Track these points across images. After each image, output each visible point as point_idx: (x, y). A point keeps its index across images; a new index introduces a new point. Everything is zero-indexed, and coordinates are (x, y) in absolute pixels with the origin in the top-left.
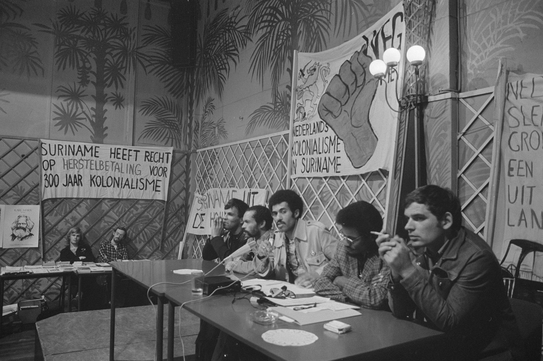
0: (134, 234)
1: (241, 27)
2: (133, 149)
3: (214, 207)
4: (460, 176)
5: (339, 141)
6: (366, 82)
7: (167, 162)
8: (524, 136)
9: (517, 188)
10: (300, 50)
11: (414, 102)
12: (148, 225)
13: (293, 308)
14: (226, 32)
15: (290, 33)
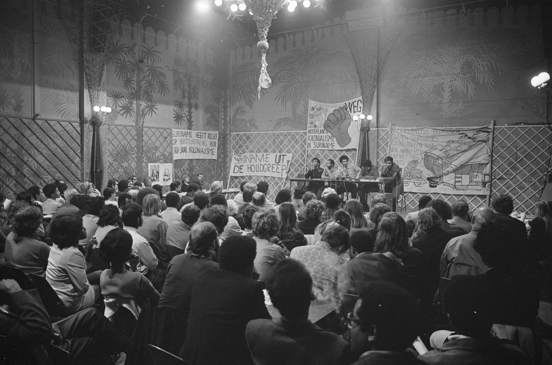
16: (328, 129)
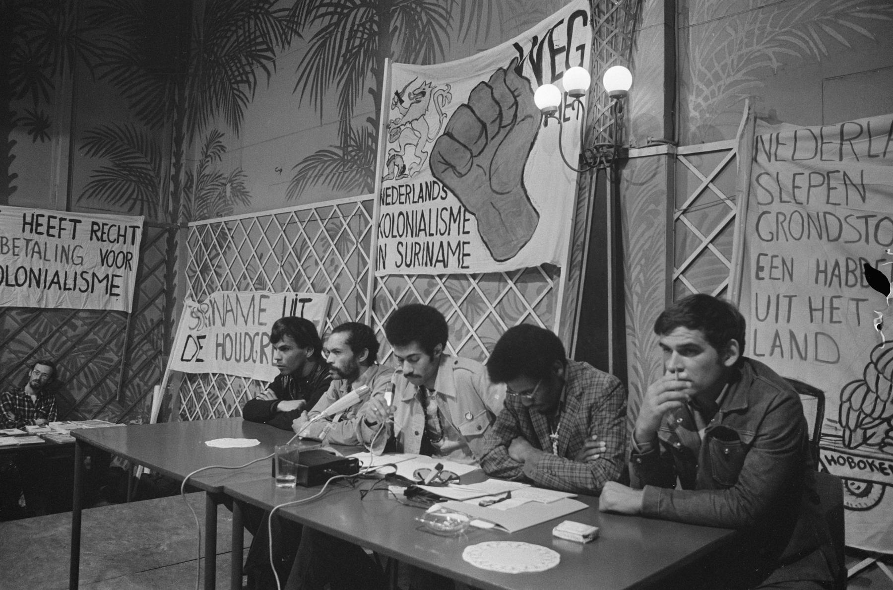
0: (68, 373)
1: (280, 10)
2: (68, 218)
3: (223, 325)
4: (678, 278)
5: (468, 216)
6: (518, 120)
7: (133, 243)
8: (781, 218)
9: (769, 297)
10: (395, 57)
11: (606, 157)
12: (95, 356)
13: (476, 502)
14: (249, 18)
15: (375, 28)
16: (451, 178)
